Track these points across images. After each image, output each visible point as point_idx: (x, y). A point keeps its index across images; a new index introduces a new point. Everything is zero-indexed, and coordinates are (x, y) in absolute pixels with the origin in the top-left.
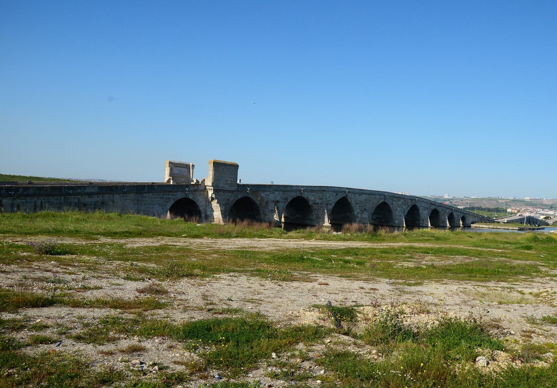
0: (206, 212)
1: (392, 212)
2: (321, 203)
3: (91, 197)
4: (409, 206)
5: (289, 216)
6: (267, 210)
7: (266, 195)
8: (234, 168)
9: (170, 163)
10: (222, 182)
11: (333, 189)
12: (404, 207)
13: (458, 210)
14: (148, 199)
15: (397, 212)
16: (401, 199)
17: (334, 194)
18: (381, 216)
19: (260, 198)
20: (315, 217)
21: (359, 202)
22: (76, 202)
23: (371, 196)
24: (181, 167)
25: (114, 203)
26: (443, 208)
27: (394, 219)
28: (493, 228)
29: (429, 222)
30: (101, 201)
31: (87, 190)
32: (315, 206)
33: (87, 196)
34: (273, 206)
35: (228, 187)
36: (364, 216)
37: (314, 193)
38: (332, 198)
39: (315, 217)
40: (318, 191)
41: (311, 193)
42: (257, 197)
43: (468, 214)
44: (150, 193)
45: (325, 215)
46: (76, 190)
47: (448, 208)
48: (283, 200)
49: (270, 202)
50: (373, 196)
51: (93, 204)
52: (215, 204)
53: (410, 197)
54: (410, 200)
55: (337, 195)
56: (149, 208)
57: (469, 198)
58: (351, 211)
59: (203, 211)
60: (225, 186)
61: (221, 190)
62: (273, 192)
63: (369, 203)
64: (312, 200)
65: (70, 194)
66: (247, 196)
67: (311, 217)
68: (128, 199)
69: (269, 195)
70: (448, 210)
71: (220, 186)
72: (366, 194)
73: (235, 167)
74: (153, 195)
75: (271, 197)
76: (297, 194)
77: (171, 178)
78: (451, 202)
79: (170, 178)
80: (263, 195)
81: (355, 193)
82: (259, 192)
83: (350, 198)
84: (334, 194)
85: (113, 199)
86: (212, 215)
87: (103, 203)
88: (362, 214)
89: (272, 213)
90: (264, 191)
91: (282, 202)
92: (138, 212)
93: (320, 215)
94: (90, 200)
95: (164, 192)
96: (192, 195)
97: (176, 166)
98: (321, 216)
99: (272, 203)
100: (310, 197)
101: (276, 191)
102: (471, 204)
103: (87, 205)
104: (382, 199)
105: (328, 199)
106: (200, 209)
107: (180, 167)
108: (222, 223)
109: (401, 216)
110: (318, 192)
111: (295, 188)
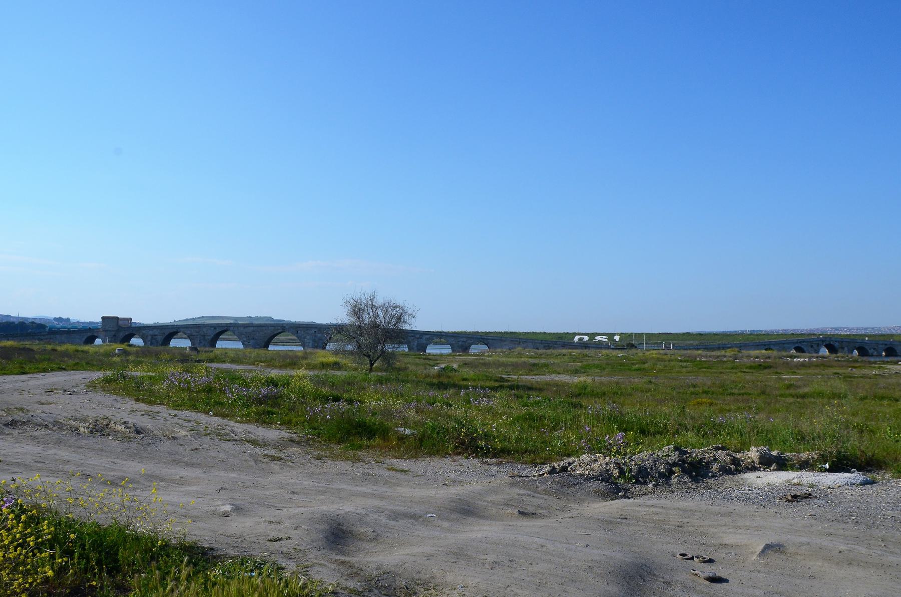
15: (306, 340)
17: (213, 329)
55: (215, 328)
75: (151, 332)
80: (144, 332)
84: (213, 329)
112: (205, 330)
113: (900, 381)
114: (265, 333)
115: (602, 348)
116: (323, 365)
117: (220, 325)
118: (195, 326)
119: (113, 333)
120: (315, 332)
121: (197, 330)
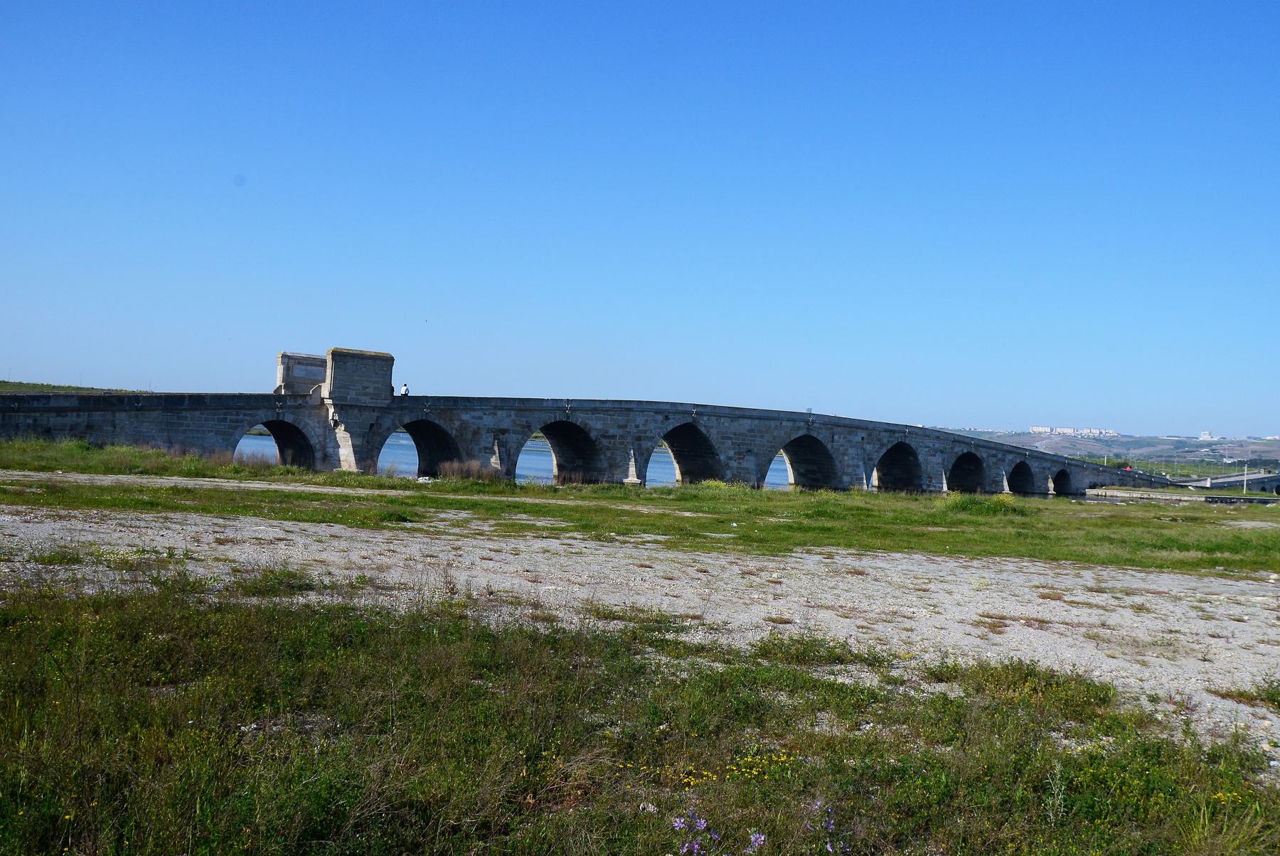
0: (325, 449)
1: (832, 458)
2: (620, 436)
3: (63, 416)
4: (883, 445)
5: (565, 464)
6: (476, 448)
7: (473, 417)
8: (384, 363)
9: (284, 356)
10: (353, 390)
11: (656, 407)
12: (868, 447)
13: (1041, 457)
14: (191, 423)
15: (846, 458)
16: (859, 430)
17: (660, 417)
18: (815, 468)
19: (457, 423)
20: (605, 465)
21: (731, 436)
22: (29, 424)
23: (768, 423)
24: (312, 365)
25: (115, 427)
26: (994, 452)
27: (839, 474)
28: (1141, 498)
29: (945, 482)
30: (86, 424)
31: (53, 404)
32: (605, 442)
33: (54, 414)
34: (491, 439)
35: (370, 401)
36: (745, 465)
37: (602, 415)
38: (652, 426)
39: (605, 465)
40: (613, 409)
41: (593, 414)
42: (451, 420)
43: (1076, 466)
44: (196, 410)
45: (629, 461)
46: (29, 403)
47: (1011, 452)
48: (518, 429)
49: (483, 432)
50: (772, 422)
51: (68, 428)
52: (341, 434)
53: (885, 427)
54: (885, 431)
55: (667, 418)
56: (193, 437)
57: (1260, 439)
58: (713, 453)
59: (318, 447)
60: (360, 398)
61: (352, 406)
62: (492, 411)
63: (762, 437)
64: (596, 429)
65: (13, 410)
66: (424, 418)
67: (599, 465)
68: (148, 422)
69: (481, 418)
70: (1010, 457)
71: (349, 397)
72: (751, 418)
73: (386, 362)
74: (202, 414)
75: (488, 421)
76: (555, 416)
77: (283, 384)
78: (1213, 450)
79: (281, 386)
80: (465, 417)
81: (721, 417)
82: (455, 412)
83: (705, 427)
84: (660, 417)
85: (114, 421)
86: (337, 455)
87: (90, 427)
88: (741, 461)
89: (486, 453)
90: (466, 409)
91: (515, 432)
92: (170, 445)
93: (618, 461)
94: (60, 420)
95: (226, 409)
96: (293, 416)
97: (299, 363)
98: (621, 463)
99: (488, 432)
100: (591, 423)
101: (499, 409)
102: (1263, 455)
103: (55, 430)
104: (799, 428)
105: (641, 428)
106: (312, 442)
107: (307, 365)
108: (354, 469)
109: (858, 466)
110: (612, 413)
111: (550, 404)
112: (640, 420)
113: (1278, 786)
114: (774, 438)
115: (230, 519)
116: (64, 557)
117: (680, 408)
118: (617, 405)
119: (371, 417)
120: (863, 438)
121: (621, 419)
